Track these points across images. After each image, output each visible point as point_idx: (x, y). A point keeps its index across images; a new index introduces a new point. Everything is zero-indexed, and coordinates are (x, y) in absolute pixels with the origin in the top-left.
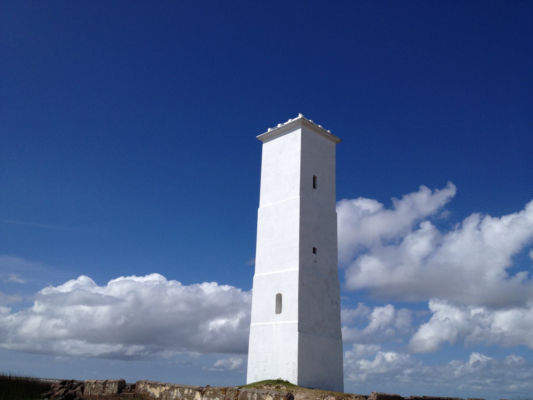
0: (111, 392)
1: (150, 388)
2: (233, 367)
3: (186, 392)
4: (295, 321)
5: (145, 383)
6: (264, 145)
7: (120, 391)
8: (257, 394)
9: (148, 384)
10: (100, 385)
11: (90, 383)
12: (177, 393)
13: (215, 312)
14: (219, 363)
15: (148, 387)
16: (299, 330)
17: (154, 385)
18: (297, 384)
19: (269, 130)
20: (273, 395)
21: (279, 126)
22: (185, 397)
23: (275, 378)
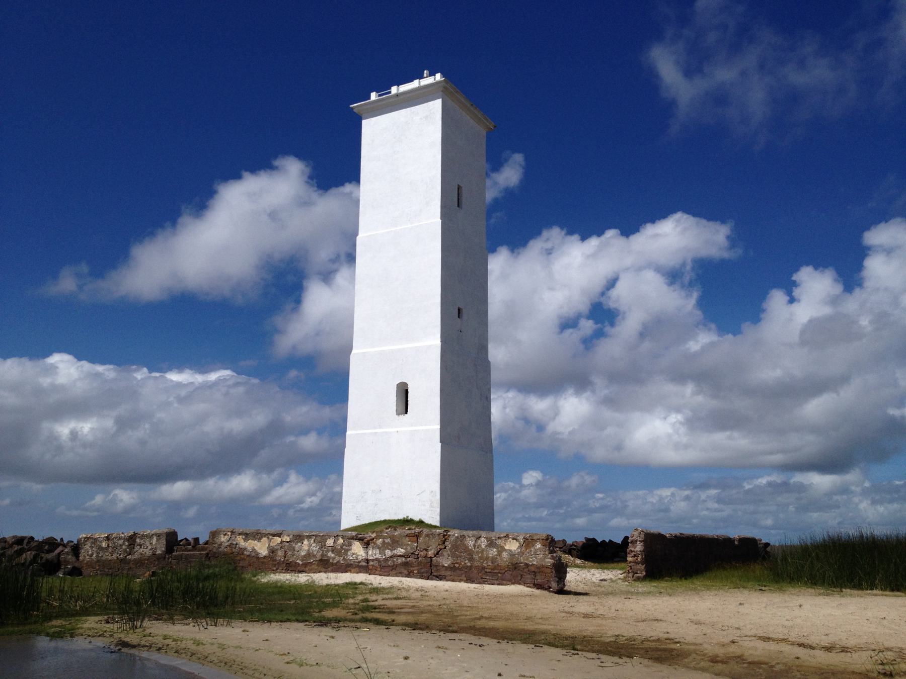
0: (148, 553)
1: (245, 540)
2: (120, 506)
3: (330, 542)
4: (435, 427)
5: (232, 532)
6: (364, 122)
7: (170, 549)
8: (486, 538)
9: (240, 534)
10: (121, 542)
11: (96, 540)
12: (310, 545)
13: (74, 407)
14: (99, 499)
15: (240, 540)
16: (442, 441)
17: (257, 535)
18: (438, 525)
19: (374, 96)
20: (521, 538)
21: (394, 90)
22: (328, 551)
23: (400, 517)
